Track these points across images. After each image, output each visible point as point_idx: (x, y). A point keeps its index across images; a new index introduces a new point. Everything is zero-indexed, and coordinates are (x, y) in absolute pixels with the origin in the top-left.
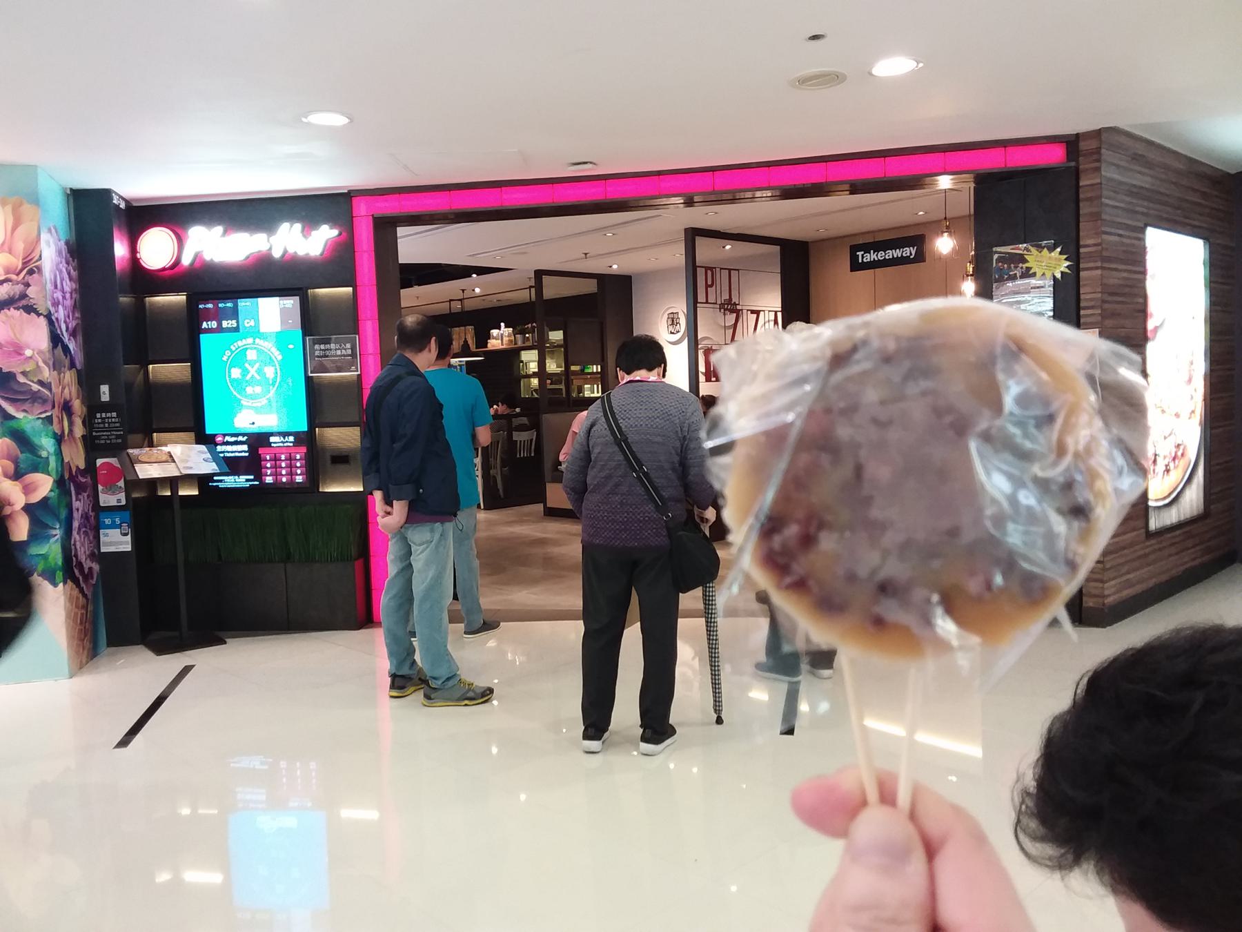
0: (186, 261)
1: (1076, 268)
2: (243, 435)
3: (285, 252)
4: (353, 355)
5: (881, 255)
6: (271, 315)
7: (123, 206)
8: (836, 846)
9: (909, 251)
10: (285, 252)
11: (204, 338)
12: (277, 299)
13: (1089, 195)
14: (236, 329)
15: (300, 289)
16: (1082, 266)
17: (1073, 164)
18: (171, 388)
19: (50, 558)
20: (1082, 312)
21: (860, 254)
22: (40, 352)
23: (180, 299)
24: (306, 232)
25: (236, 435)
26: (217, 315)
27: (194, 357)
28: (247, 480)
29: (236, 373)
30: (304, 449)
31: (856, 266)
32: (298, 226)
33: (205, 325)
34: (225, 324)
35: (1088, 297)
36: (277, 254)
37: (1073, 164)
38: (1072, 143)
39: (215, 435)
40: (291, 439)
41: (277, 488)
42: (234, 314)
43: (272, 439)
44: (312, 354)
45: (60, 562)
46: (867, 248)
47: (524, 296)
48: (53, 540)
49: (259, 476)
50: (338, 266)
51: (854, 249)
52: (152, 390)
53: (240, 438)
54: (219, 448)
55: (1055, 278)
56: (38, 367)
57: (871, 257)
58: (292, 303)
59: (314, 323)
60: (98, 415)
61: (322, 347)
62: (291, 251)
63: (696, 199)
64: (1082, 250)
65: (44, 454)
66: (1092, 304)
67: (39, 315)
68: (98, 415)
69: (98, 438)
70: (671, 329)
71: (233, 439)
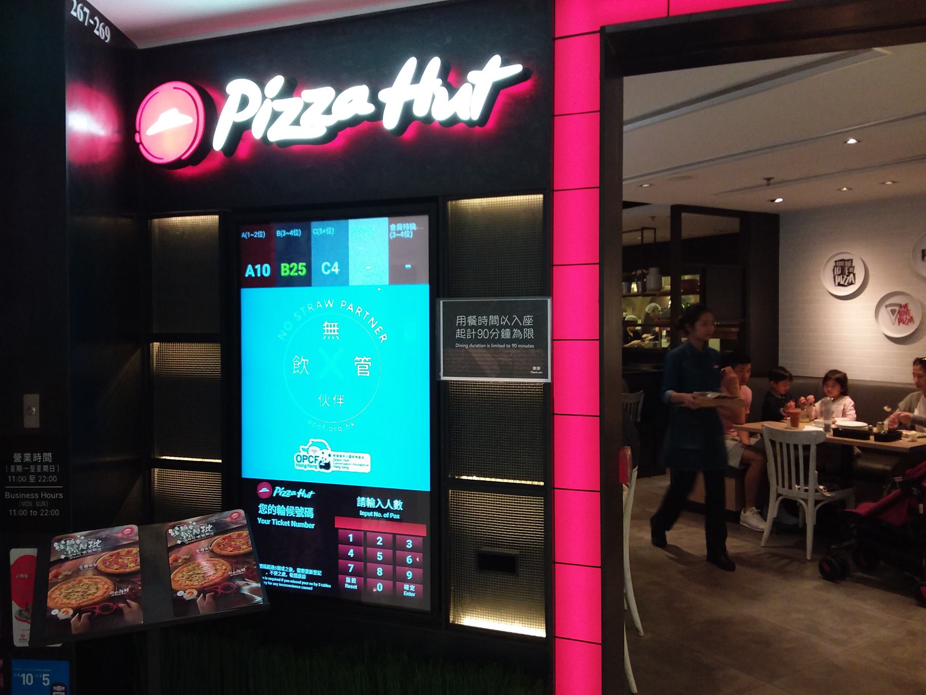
2: (308, 486)
4: (539, 339)
6: (370, 248)
7: (102, 32)
8: (386, 279)
11: (250, 298)
12: (385, 221)
14: (305, 281)
15: (433, 199)
18: (188, 384)
24: (452, 79)
25: (295, 486)
26: (266, 252)
27: (228, 335)
28: (310, 578)
29: (301, 363)
30: (422, 530)
33: (250, 271)
34: (285, 270)
39: (257, 482)
40: (398, 504)
41: (358, 608)
43: (362, 501)
44: (451, 340)
47: (664, 234)
49: (333, 573)
50: (515, 142)
52: (156, 387)
53: (301, 493)
54: (263, 508)
58: (411, 228)
59: (455, 272)
60: (17, 457)
68: (17, 457)
69: (15, 504)
70: (839, 279)
71: (288, 493)
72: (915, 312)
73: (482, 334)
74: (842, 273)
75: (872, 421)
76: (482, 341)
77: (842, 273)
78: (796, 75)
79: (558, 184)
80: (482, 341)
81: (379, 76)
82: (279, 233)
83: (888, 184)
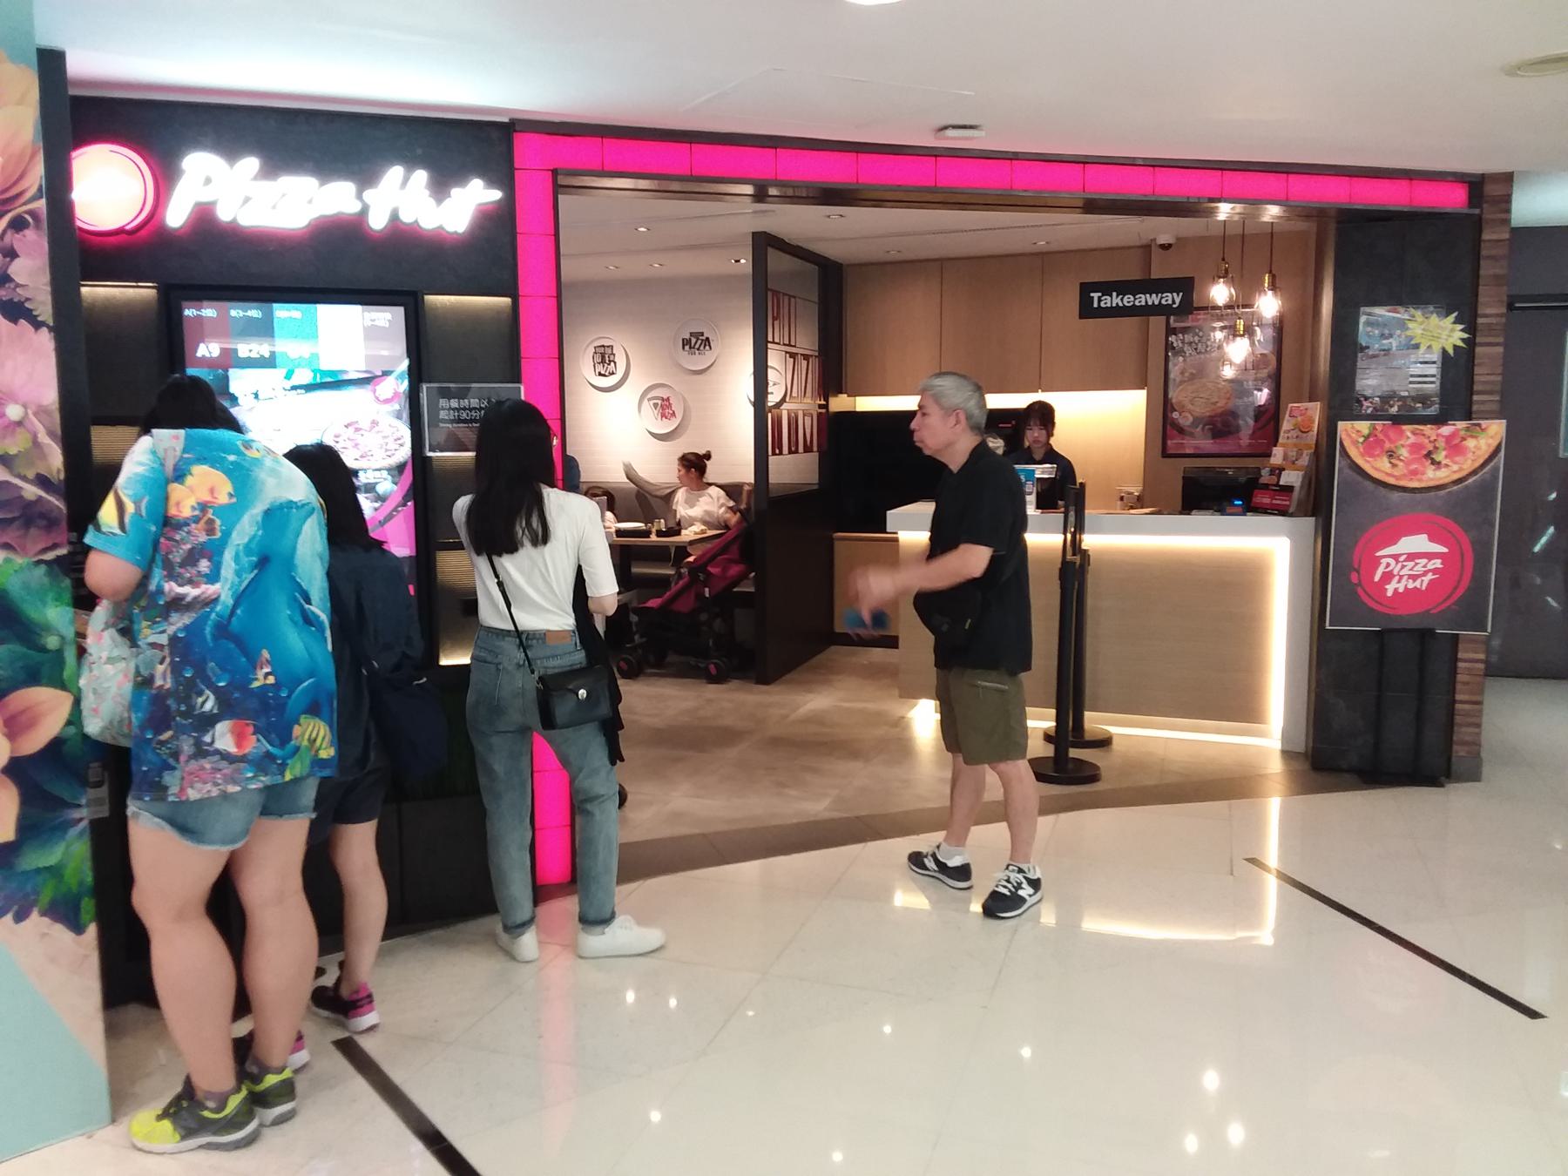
0: (176, 216)
1: (1471, 343)
3: (395, 217)
5: (1128, 300)
9: (1172, 299)
10: (395, 217)
13: (1493, 252)
16: (1478, 340)
17: (1477, 211)
19: (68, 873)
20: (1475, 398)
21: (1095, 295)
22: (41, 411)
23: (141, 293)
24: (440, 187)
31: (1087, 311)
32: (421, 176)
35: (1483, 379)
36: (377, 222)
37: (1477, 211)
38: (1476, 185)
42: (265, 329)
44: (435, 421)
45: (89, 878)
46: (1106, 288)
48: (73, 832)
51: (1086, 289)
55: (1444, 352)
56: (36, 443)
57: (1113, 300)
61: (454, 403)
62: (407, 218)
63: (773, 191)
64: (1480, 321)
65: (52, 642)
66: (1488, 388)
67: (37, 325)
70: (600, 368)
72: (677, 407)
73: (464, 415)
74: (603, 361)
75: (648, 519)
76: (465, 421)
77: (603, 361)
78: (1318, 595)
79: (523, 289)
80: (465, 421)
81: (366, 177)
82: (233, 313)
83: (657, 266)
